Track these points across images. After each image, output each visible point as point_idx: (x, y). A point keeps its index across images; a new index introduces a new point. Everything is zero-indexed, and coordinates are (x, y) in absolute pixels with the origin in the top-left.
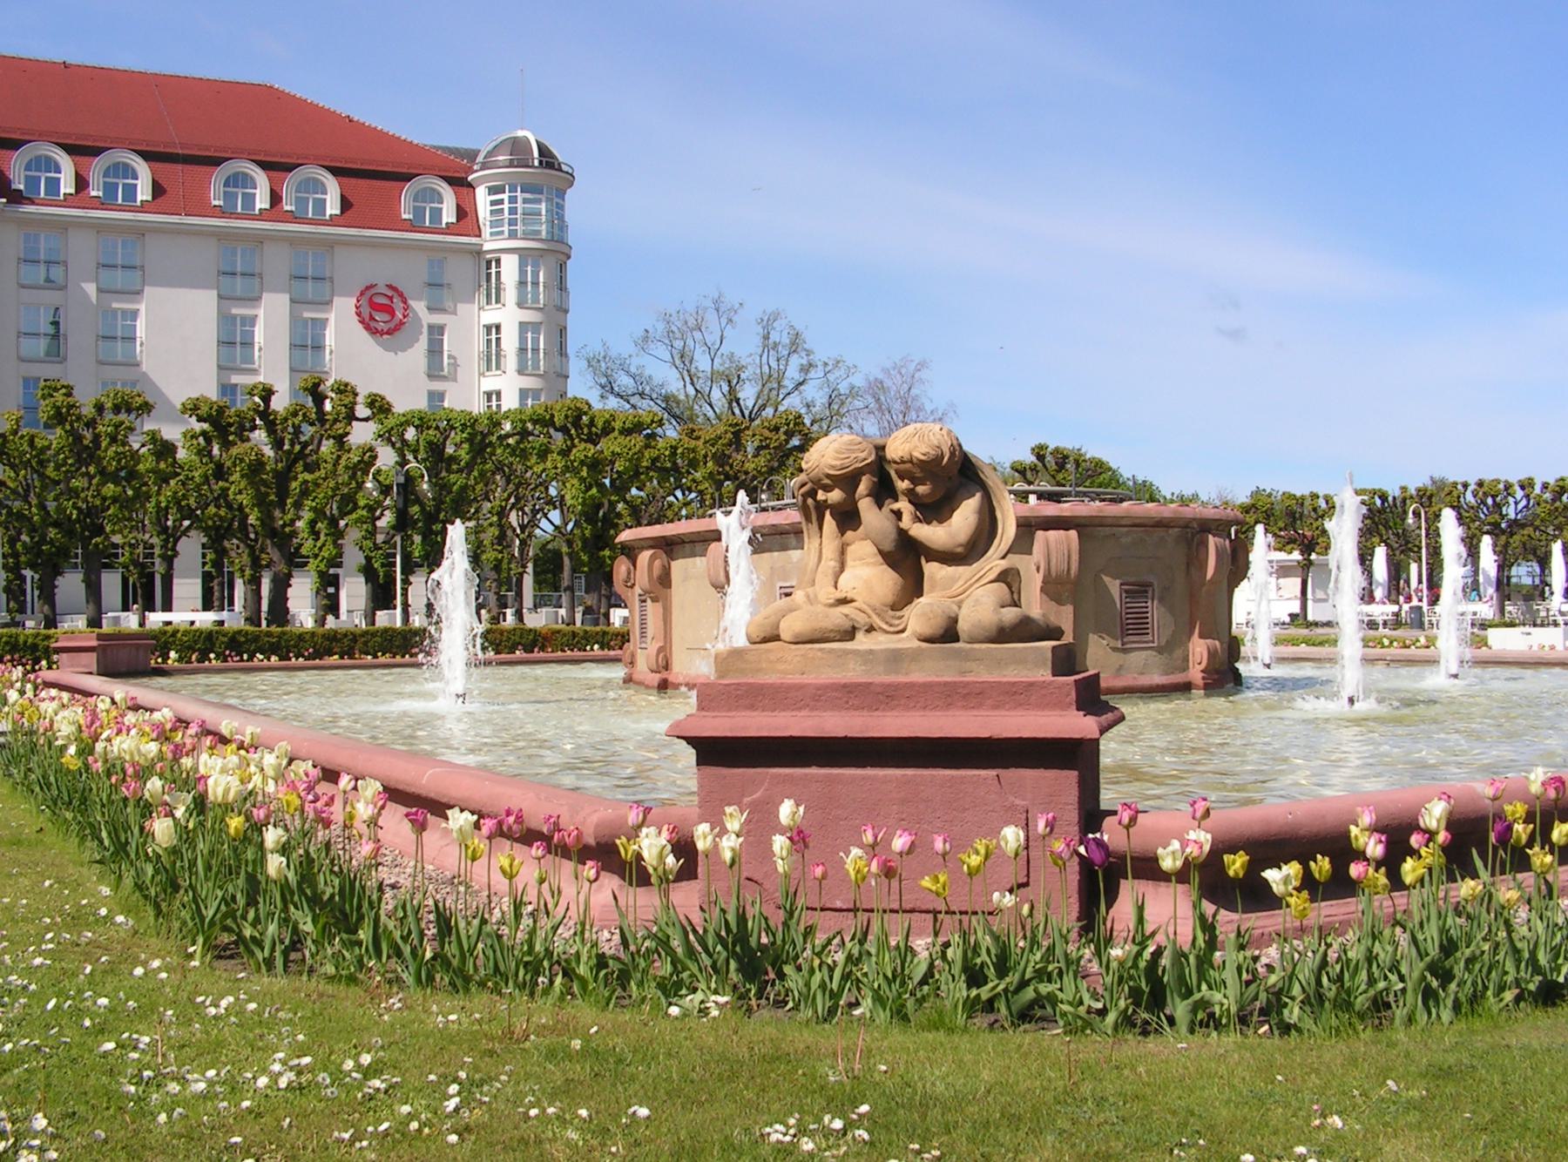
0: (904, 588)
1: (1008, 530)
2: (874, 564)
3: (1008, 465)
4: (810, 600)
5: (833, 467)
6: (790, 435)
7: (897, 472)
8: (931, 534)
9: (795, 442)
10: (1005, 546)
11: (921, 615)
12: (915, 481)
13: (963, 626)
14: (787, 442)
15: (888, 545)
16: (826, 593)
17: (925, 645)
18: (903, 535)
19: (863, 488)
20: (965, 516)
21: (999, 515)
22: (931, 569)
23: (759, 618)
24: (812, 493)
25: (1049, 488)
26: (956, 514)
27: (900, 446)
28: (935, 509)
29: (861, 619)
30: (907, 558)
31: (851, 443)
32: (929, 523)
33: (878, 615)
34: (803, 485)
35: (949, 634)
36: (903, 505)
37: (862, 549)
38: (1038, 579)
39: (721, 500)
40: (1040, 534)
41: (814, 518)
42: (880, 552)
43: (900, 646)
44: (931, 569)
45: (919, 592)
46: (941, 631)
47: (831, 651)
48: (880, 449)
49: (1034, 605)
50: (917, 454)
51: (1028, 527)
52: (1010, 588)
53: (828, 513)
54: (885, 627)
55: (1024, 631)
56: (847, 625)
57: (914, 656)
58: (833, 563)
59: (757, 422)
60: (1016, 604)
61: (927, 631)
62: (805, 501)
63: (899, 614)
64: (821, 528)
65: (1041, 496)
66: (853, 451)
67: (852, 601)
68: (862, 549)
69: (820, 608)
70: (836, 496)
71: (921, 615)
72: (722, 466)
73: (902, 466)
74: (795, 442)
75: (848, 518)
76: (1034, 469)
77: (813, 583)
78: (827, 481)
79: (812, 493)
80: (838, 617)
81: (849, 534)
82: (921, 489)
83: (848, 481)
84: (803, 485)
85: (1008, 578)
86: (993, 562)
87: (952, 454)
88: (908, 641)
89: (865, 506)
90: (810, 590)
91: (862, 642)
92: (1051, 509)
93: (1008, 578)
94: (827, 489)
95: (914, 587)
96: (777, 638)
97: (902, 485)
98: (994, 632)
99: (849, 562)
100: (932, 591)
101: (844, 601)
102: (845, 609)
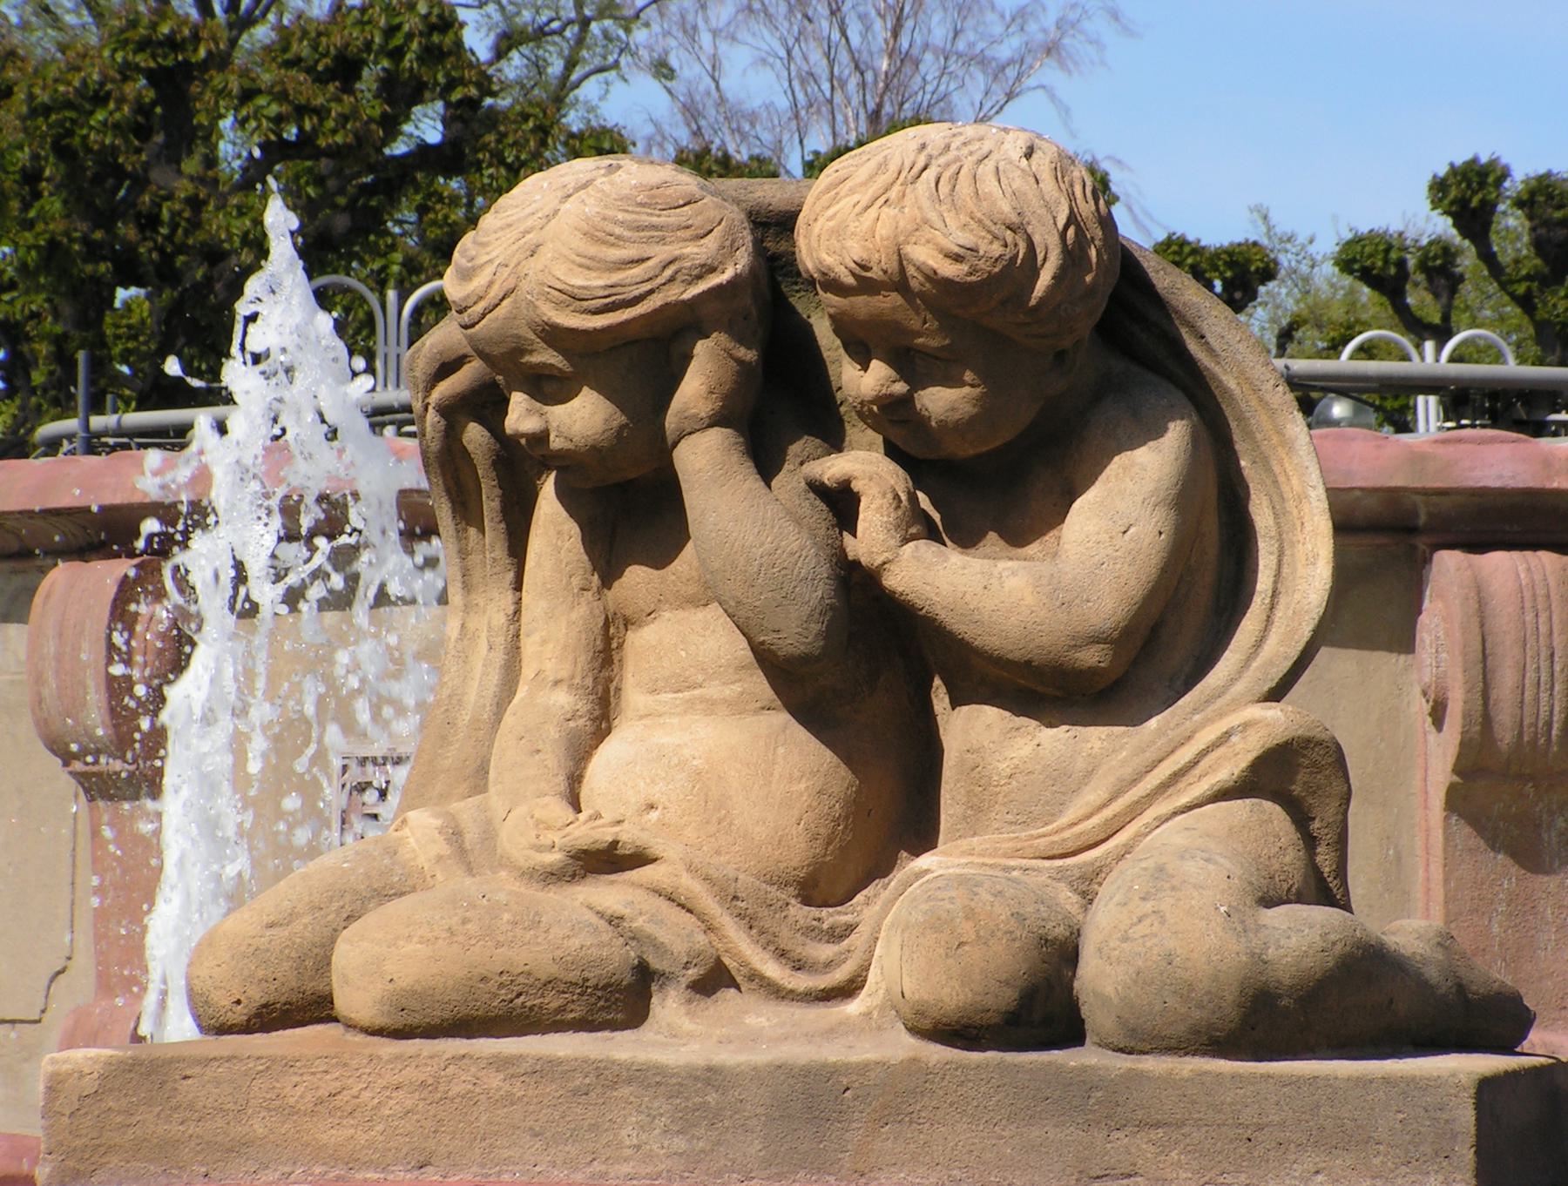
0: (856, 810)
1: (1299, 563)
2: (736, 707)
3: (1327, 245)
4: (462, 850)
5: (574, 298)
6: (402, 95)
7: (841, 325)
8: (975, 587)
9: (427, 126)
10: (1280, 649)
11: (922, 928)
12: (914, 365)
13: (1100, 979)
14: (391, 126)
15: (796, 631)
16: (531, 822)
17: (937, 1053)
18: (858, 587)
19: (698, 385)
20: (1118, 518)
21: (1261, 515)
22: (972, 733)
23: (245, 923)
24: (486, 403)
25: (1511, 368)
26: (1084, 508)
27: (855, 218)
28: (994, 486)
29: (676, 937)
30: (871, 682)
31: (652, 199)
32: (966, 539)
33: (749, 921)
34: (446, 369)
35: (1039, 1008)
36: (864, 464)
37: (687, 645)
38: (1437, 757)
39: (99, 366)
40: (1449, 565)
41: (491, 505)
42: (767, 660)
43: (832, 1053)
44: (972, 733)
45: (919, 829)
46: (1007, 998)
47: (546, 1069)
48: (775, 226)
49: (1414, 889)
50: (924, 255)
51: (1387, 544)
52: (1300, 817)
53: (548, 489)
54: (773, 970)
55: (1361, 1006)
56: (616, 958)
57: (892, 1099)
58: (563, 699)
59: (262, 33)
60: (1325, 890)
61: (951, 995)
62: (452, 434)
63: (832, 917)
64: (517, 547)
65: (1461, 402)
66: (658, 233)
67: (640, 859)
68: (687, 645)
69: (505, 887)
70: (583, 417)
71: (922, 928)
72: (106, 219)
73: (862, 305)
74: (427, 126)
75: (632, 512)
76: (1440, 268)
77: (478, 778)
78: (545, 356)
79: (486, 403)
80: (577, 925)
81: (637, 579)
82: (941, 401)
83: (638, 356)
84: (446, 369)
85: (1293, 778)
86: (1228, 714)
87: (1073, 257)
88: (864, 1038)
89: (706, 463)
90: (465, 809)
91: (677, 1034)
92: (1499, 461)
93: (1293, 778)
94: (549, 387)
95: (897, 805)
96: (313, 1008)
97: (863, 381)
98: (1230, 1012)
99: (634, 696)
100: (944, 853)
101: (606, 860)
102: (610, 894)
